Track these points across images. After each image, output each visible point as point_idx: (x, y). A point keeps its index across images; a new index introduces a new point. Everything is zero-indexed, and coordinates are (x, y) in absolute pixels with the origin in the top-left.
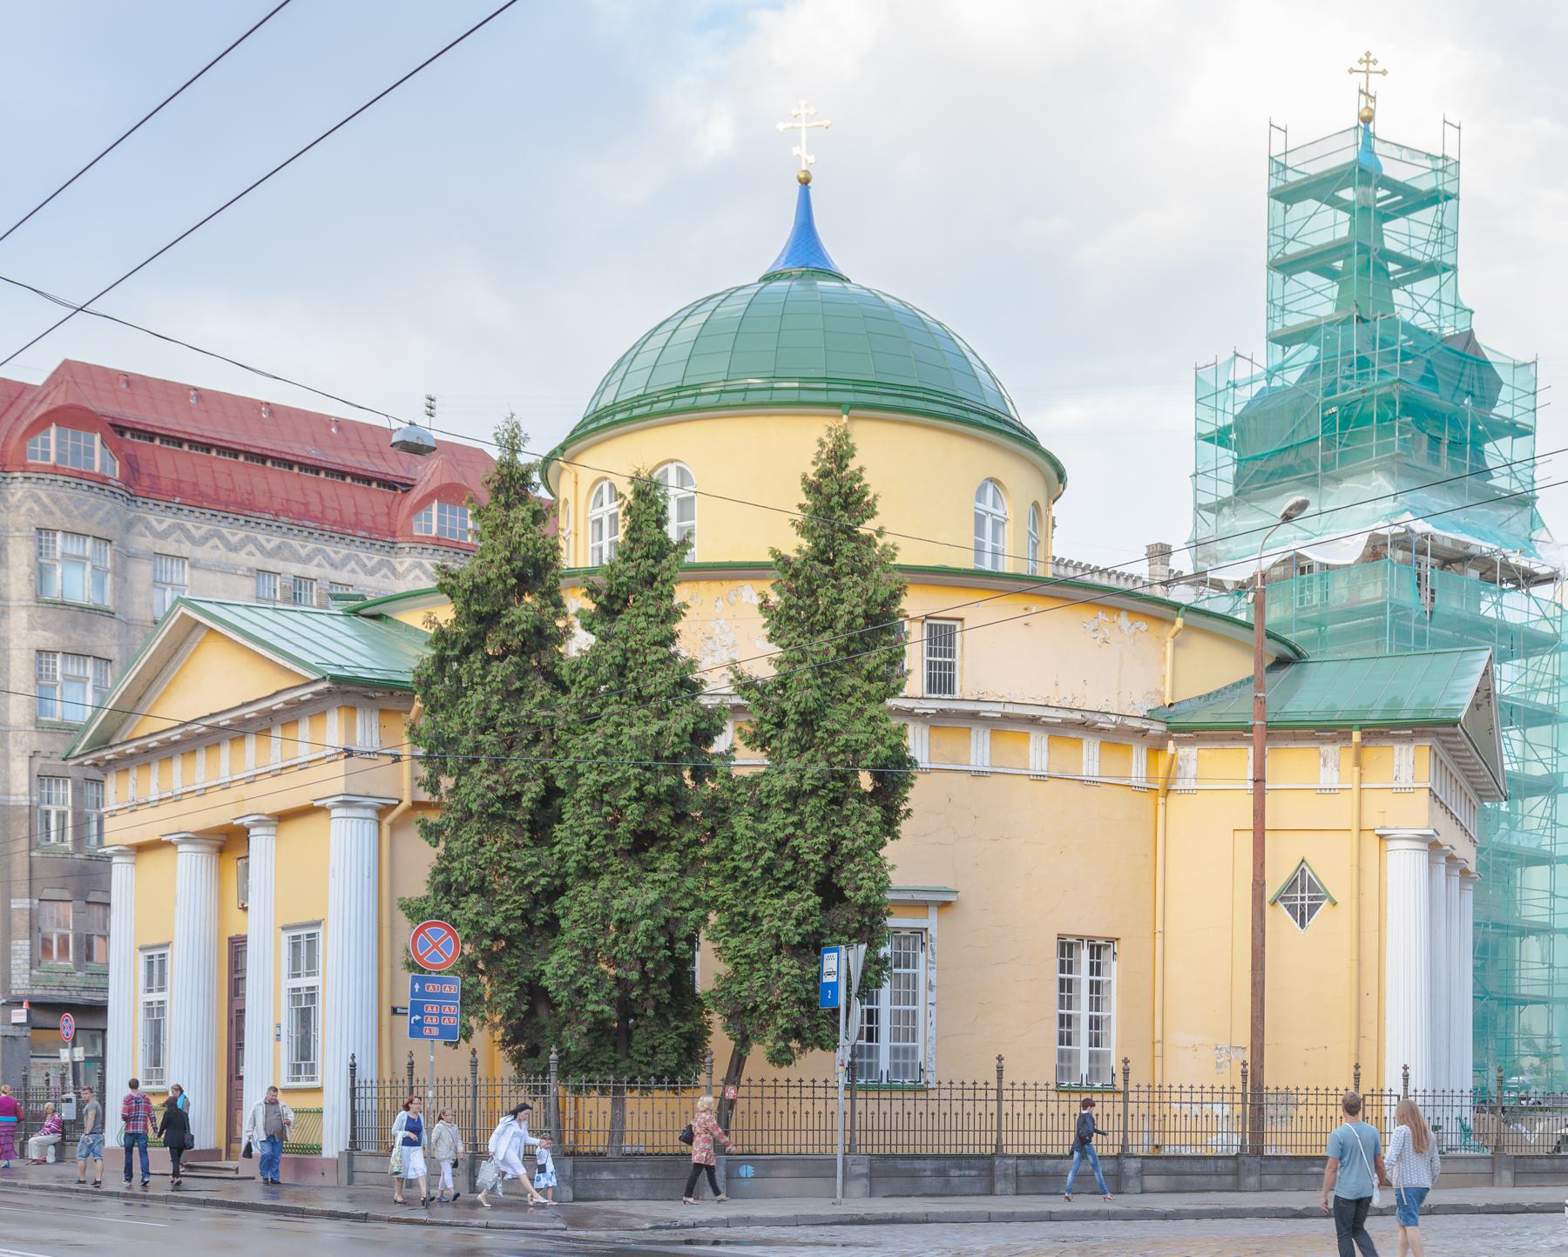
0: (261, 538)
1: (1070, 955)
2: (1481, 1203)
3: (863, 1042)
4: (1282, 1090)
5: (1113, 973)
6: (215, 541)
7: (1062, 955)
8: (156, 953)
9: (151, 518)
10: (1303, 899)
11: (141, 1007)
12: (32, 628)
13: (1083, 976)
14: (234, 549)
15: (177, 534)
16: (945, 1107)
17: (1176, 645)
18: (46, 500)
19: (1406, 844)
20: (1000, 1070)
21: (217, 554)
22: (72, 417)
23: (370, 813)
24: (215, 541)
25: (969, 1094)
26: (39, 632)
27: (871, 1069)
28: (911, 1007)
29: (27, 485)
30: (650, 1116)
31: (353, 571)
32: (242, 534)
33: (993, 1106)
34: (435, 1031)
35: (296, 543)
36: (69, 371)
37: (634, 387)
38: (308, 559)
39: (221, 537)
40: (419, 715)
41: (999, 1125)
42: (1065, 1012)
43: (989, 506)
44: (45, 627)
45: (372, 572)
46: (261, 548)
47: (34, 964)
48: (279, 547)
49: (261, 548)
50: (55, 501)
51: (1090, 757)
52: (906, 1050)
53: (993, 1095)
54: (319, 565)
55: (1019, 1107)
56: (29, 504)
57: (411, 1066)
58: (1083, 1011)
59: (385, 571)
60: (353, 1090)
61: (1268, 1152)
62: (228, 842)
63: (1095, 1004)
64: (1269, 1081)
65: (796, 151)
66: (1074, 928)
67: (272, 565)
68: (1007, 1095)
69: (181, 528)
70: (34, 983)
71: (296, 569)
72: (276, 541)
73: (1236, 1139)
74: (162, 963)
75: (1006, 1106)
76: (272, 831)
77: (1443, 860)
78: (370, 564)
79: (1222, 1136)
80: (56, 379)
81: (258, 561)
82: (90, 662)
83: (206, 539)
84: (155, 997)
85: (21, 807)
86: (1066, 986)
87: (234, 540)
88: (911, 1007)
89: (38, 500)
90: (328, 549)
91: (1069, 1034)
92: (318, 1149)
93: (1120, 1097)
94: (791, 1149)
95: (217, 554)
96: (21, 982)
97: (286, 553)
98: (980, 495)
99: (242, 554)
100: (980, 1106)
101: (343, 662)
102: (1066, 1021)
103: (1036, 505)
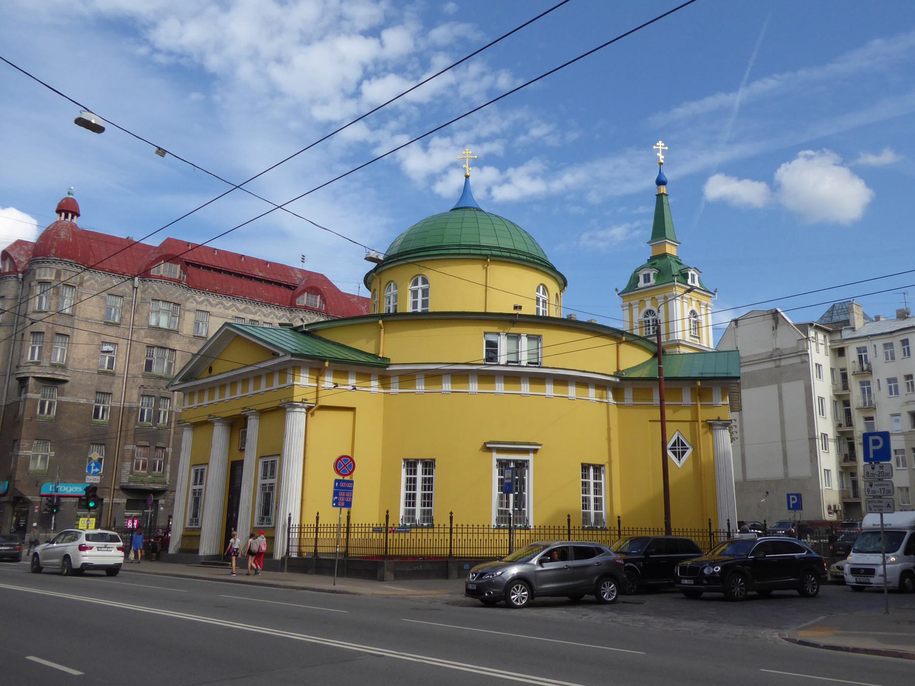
8: (200, 468)
13: (419, 476)
14: (227, 309)
15: (206, 303)
20: (569, 521)
21: (220, 311)
22: (171, 258)
23: (304, 410)
27: (413, 520)
34: (343, 504)
36: (169, 242)
37: (395, 251)
38: (255, 313)
39: (222, 304)
40: (684, 336)
43: (541, 294)
46: (238, 309)
47: (132, 472)
51: (592, 393)
53: (566, 532)
55: (459, 536)
57: (729, 524)
62: (237, 425)
66: (587, 461)
69: (208, 300)
71: (250, 317)
72: (243, 306)
74: (202, 473)
75: (454, 536)
80: (163, 245)
82: (167, 351)
84: (198, 487)
86: (585, 484)
87: (228, 305)
92: (197, 551)
95: (220, 311)
98: (538, 290)
100: (441, 536)
102: (585, 500)
103: (557, 295)
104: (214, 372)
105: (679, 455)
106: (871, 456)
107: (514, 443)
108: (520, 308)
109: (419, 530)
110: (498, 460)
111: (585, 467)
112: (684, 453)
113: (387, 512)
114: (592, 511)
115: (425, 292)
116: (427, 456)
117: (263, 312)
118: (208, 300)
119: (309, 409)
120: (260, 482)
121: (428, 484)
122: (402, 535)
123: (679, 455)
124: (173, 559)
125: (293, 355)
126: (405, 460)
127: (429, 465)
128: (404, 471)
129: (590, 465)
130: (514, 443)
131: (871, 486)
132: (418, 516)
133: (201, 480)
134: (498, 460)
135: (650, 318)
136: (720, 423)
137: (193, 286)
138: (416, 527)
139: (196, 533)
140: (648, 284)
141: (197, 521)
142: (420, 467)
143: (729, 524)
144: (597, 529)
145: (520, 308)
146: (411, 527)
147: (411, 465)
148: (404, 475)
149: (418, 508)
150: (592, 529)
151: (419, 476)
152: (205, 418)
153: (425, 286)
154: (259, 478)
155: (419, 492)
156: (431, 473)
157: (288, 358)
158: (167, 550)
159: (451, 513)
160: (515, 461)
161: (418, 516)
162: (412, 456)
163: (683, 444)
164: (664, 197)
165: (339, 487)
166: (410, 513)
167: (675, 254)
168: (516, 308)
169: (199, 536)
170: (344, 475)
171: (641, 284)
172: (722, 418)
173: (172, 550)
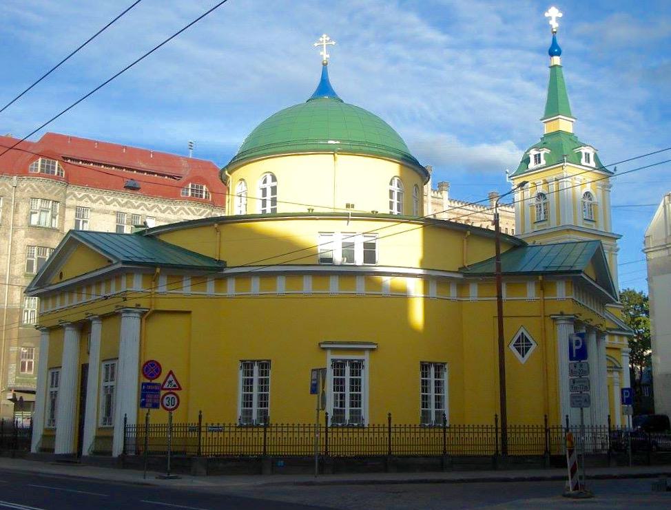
0: (120, 199)
1: (426, 370)
2: (593, 475)
3: (338, 408)
4: (485, 426)
5: (446, 377)
6: (101, 201)
7: (423, 369)
8: (110, 363)
9: (76, 193)
10: (523, 345)
11: (48, 393)
12: (26, 236)
13: (256, 377)
15: (86, 199)
16: (462, 435)
17: (467, 241)
18: (35, 187)
19: (564, 322)
20: (390, 419)
24: (101, 201)
25: (376, 430)
26: (29, 239)
27: (342, 420)
28: (358, 393)
29: (28, 182)
30: (217, 439)
31: (156, 212)
32: (112, 198)
33: (387, 435)
34: (151, 405)
35: (133, 201)
36: (50, 137)
38: (138, 207)
41: (326, 443)
42: (425, 394)
44: (31, 237)
45: (163, 212)
46: (119, 203)
47: (17, 374)
48: (127, 203)
49: (119, 203)
50: (39, 187)
52: (356, 411)
53: (387, 430)
54: (142, 210)
56: (29, 188)
57: (567, 420)
58: (432, 394)
59: (169, 211)
60: (125, 429)
61: (509, 454)
62: (83, 328)
63: (438, 390)
64: (510, 421)
65: (321, 53)
67: (124, 210)
68: (393, 430)
69: (88, 196)
70: (17, 381)
71: (132, 211)
73: (494, 448)
75: (393, 435)
76: (101, 322)
77: (584, 327)
78: (163, 209)
79: (486, 445)
80: (42, 141)
81: (117, 208)
83: (97, 200)
84: (110, 384)
85: (16, 309)
86: (425, 383)
88: (358, 393)
89: (32, 187)
90: (146, 203)
91: (426, 403)
92: (110, 453)
93: (442, 430)
94: (294, 454)
96: (12, 382)
97: (129, 205)
99: (112, 206)
101: (139, 255)
104: (63, 279)
105: (523, 352)
106: (574, 356)
107: (349, 343)
108: (353, 206)
109: (256, 430)
110: (333, 360)
111: (425, 367)
112: (527, 349)
113: (200, 412)
114: (433, 409)
115: (274, 190)
116: (263, 357)
117: (145, 206)
118: (88, 196)
119: (143, 314)
120: (103, 384)
121: (264, 383)
122: (215, 434)
123: (523, 352)
124: (36, 457)
125: (124, 262)
126: (242, 361)
127: (265, 366)
128: (241, 372)
129: (431, 363)
130: (349, 343)
131: (574, 382)
132: (255, 416)
133: (57, 383)
134: (333, 360)
135: (542, 201)
136: (564, 317)
137: (68, 181)
138: (252, 426)
139: (52, 434)
140: (539, 165)
141: (110, 420)
142: (256, 368)
143: (567, 420)
144: (353, 427)
145: (353, 206)
146: (247, 427)
147: (247, 366)
148: (241, 376)
149: (255, 408)
150: (348, 427)
151: (347, 377)
152: (57, 323)
153: (274, 184)
154: (102, 381)
155: (256, 392)
156: (267, 374)
157: (120, 265)
158: (30, 449)
159: (390, 414)
160: (351, 361)
161: (255, 416)
162: (249, 357)
163: (527, 340)
164: (558, 69)
165: (146, 390)
166: (248, 413)
167: (571, 131)
168: (348, 206)
169: (55, 436)
170: (151, 379)
171: (532, 165)
172: (565, 313)
173: (34, 450)
